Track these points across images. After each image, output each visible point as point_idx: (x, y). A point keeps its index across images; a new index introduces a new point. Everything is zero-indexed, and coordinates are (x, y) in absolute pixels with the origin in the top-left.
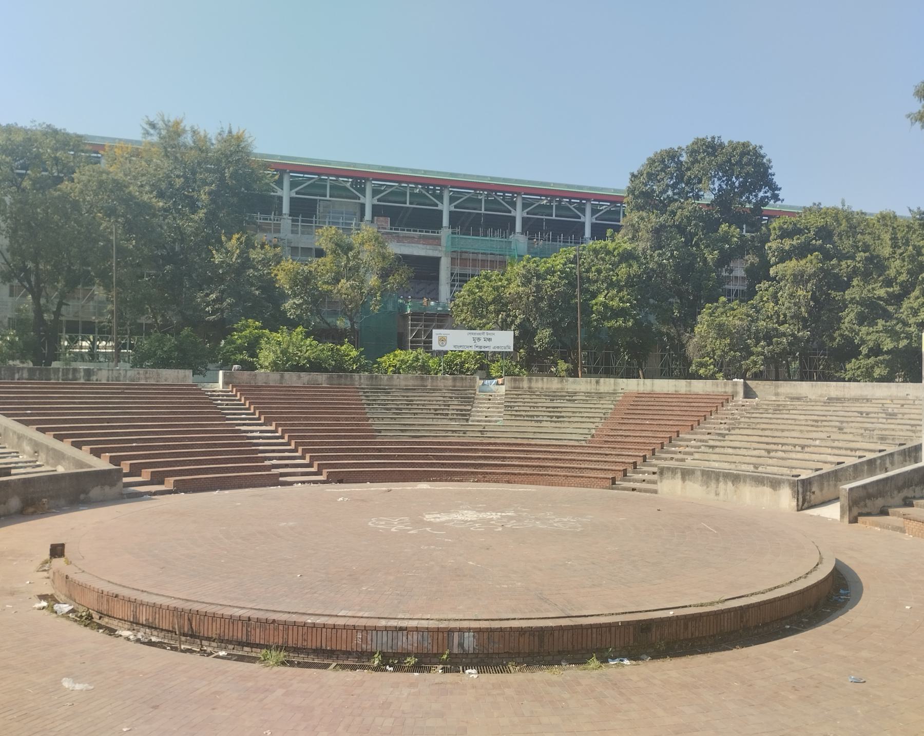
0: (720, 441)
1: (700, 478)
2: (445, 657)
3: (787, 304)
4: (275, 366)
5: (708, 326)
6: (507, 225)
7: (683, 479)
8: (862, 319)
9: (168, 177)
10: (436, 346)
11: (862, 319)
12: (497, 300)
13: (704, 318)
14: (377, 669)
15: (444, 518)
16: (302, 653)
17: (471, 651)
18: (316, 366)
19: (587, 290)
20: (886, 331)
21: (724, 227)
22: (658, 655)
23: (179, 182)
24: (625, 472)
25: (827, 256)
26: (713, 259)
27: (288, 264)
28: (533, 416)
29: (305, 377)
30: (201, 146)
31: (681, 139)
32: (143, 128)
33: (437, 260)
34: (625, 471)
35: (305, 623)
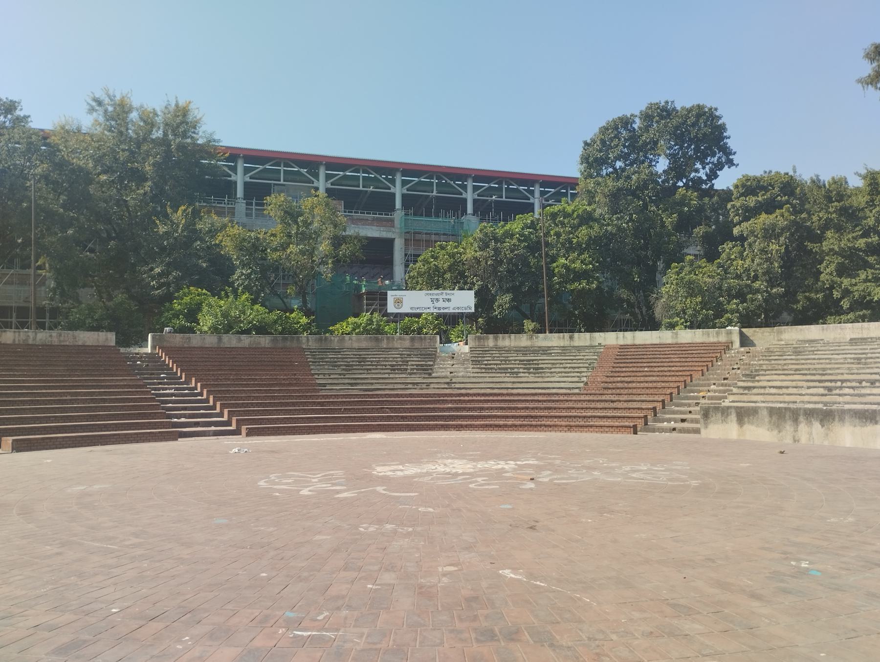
1: (767, 420)
4: (214, 329)
7: (740, 420)
8: (842, 271)
10: (391, 308)
11: (842, 271)
15: (411, 470)
18: (262, 329)
23: (122, 156)
25: (796, 212)
26: (672, 223)
28: (507, 369)
29: (246, 341)
30: (149, 121)
31: (633, 106)
32: (88, 104)
33: (391, 242)
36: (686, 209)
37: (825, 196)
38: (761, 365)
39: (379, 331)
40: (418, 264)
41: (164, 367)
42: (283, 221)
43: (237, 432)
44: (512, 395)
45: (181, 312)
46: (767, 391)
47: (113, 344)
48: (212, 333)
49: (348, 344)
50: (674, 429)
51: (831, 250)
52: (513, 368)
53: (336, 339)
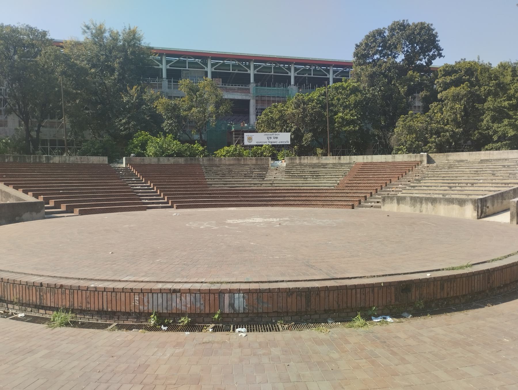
0: (418, 183)
1: (409, 202)
2: (216, 316)
3: (449, 113)
4: (156, 155)
5: (402, 127)
6: (285, 81)
7: (398, 203)
8: (494, 120)
9: (97, 55)
10: (246, 143)
11: (494, 120)
12: (281, 118)
13: (400, 123)
14: (154, 328)
16: (87, 314)
17: (242, 310)
18: (179, 154)
19: (332, 111)
20: (510, 125)
21: (410, 72)
22: (418, 313)
23: (102, 58)
24: (360, 202)
25: (472, 85)
27: (164, 100)
28: (302, 176)
29: (172, 160)
31: (384, 23)
32: (82, 29)
33: (248, 101)
34: (360, 201)
35: (88, 288)
36: (412, 83)
37: (488, 77)
38: (428, 174)
39: (240, 155)
40: (263, 116)
41: (133, 175)
42: (188, 94)
43: (172, 207)
44: (301, 189)
45: (138, 145)
46: (422, 188)
47: (107, 163)
48: (154, 156)
49: (223, 162)
50: (372, 206)
51: (488, 108)
52: (305, 176)
53: (218, 159)
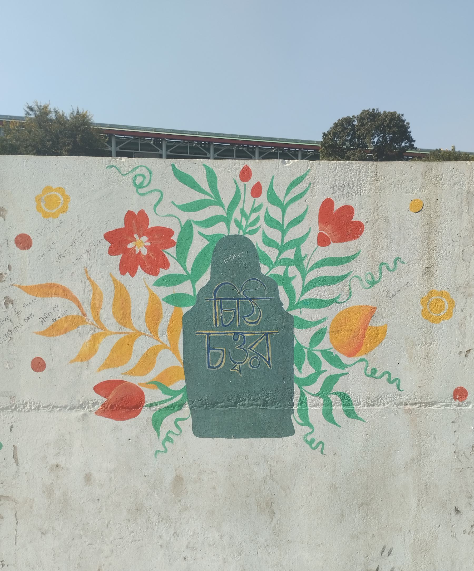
31: (354, 111)
32: (25, 111)
